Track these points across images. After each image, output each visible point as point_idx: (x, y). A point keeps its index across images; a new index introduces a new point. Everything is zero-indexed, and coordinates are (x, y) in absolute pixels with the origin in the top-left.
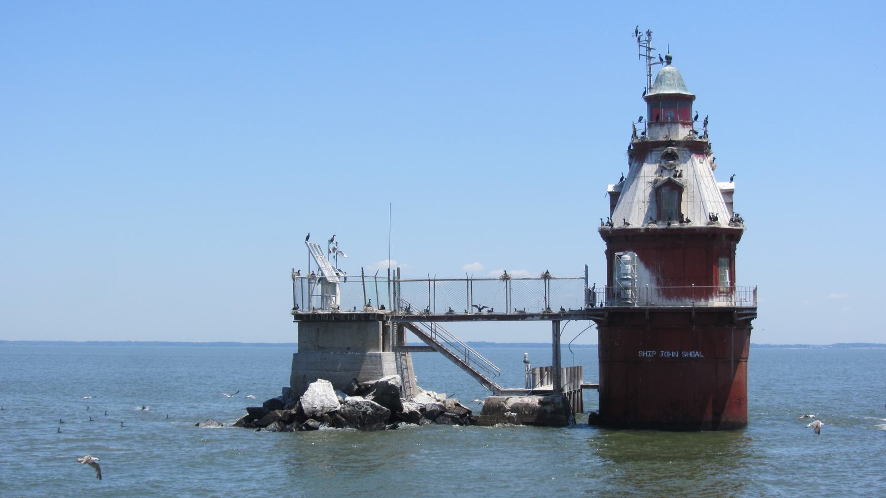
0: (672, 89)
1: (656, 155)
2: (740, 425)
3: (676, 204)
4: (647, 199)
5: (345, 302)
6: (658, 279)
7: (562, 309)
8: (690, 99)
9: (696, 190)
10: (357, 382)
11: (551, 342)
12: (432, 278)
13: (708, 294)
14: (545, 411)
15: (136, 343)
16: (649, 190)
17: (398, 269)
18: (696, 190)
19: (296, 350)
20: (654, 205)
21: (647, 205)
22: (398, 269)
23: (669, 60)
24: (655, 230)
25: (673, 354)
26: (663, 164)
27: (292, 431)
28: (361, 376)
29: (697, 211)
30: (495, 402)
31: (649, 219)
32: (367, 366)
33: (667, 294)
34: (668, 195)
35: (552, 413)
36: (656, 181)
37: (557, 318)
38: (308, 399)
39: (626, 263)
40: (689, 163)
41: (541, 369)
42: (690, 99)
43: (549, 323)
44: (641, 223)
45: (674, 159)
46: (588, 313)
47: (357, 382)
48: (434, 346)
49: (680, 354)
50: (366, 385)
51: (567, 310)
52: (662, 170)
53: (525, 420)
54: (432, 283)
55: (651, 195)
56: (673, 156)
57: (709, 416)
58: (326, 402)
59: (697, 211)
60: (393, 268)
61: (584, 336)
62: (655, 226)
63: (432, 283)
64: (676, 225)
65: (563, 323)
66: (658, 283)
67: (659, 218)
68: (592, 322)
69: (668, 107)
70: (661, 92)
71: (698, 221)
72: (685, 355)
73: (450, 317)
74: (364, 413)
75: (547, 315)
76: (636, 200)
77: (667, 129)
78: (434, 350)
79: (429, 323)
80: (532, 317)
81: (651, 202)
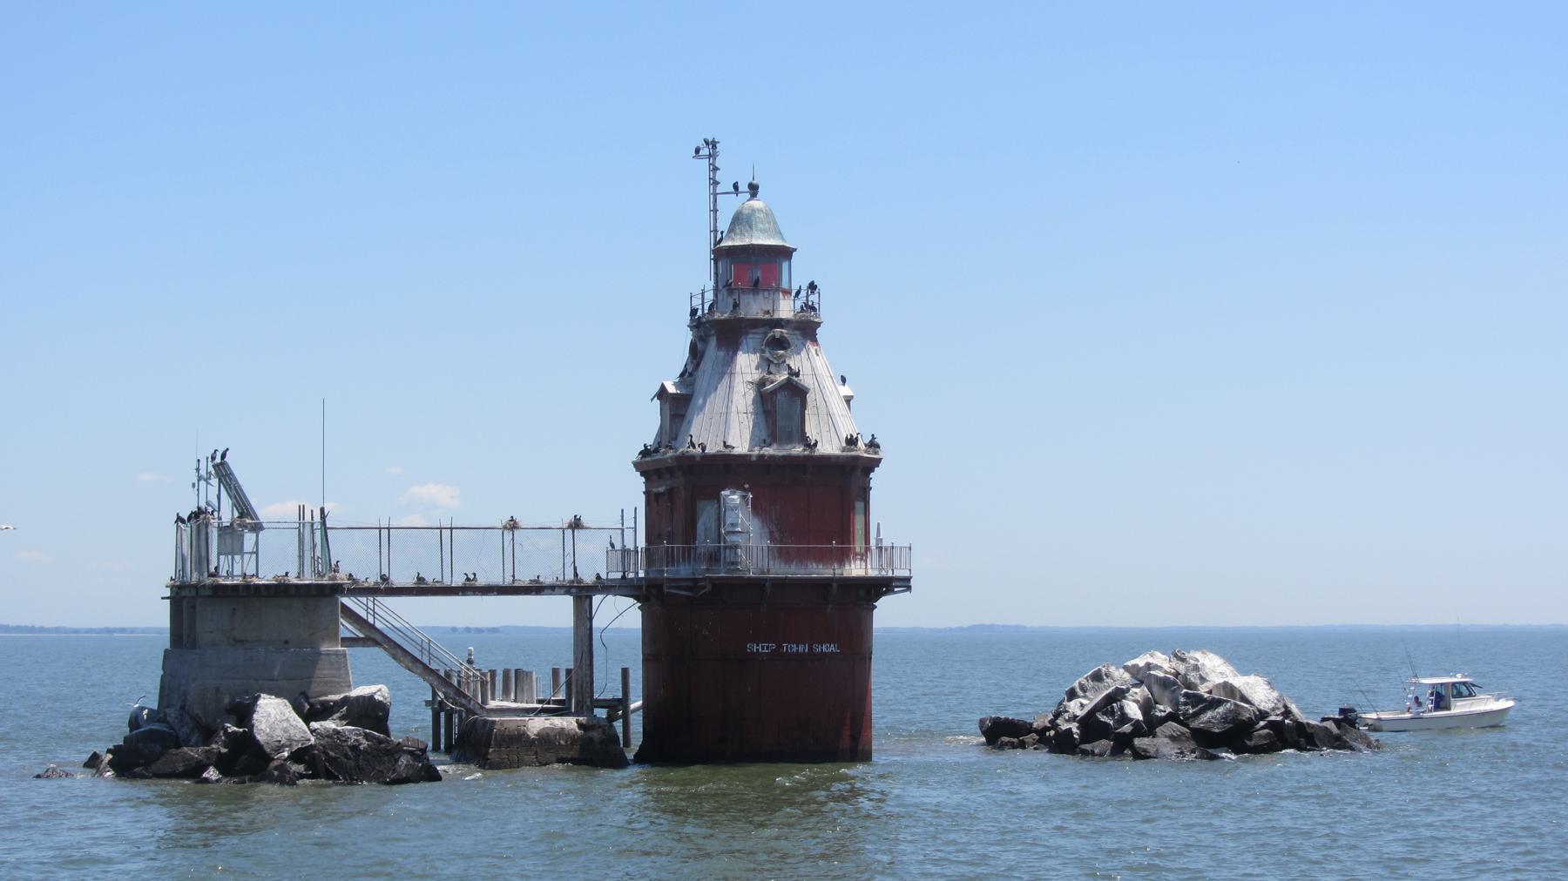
0: (770, 237)
1: (752, 339)
2: (859, 752)
3: (797, 418)
4: (750, 409)
5: (273, 560)
6: (771, 533)
7: (598, 577)
8: (786, 253)
9: (819, 397)
10: (307, 698)
11: (640, 625)
12: (384, 524)
13: (844, 556)
14: (591, 740)
15: (58, 630)
16: (751, 395)
17: (322, 510)
18: (819, 397)
19: (166, 642)
20: (762, 418)
21: (751, 418)
22: (322, 510)
23: (754, 189)
24: (772, 457)
25: (801, 649)
26: (767, 355)
27: (434, 776)
28: (315, 688)
29: (824, 429)
30: (512, 727)
31: (755, 440)
32: (323, 671)
33: (785, 556)
34: (782, 404)
35: (602, 742)
36: (761, 384)
37: (582, 593)
38: (263, 726)
39: (735, 508)
40: (804, 353)
41: (506, 673)
42: (786, 253)
43: (568, 600)
44: (747, 445)
45: (784, 348)
46: (623, 587)
47: (307, 698)
48: (378, 637)
49: (811, 648)
50: (324, 703)
51: (429, 580)
52: (767, 364)
53: (562, 754)
54: (385, 532)
55: (754, 401)
56: (782, 344)
57: (846, 743)
58: (292, 732)
59: (824, 429)
60: (313, 508)
61: (620, 617)
62: (769, 451)
63: (446, 533)
64: (798, 450)
65: (597, 599)
66: (772, 539)
67: (773, 437)
68: (632, 601)
69: (748, 266)
70: (755, 242)
71: (829, 446)
72: (818, 649)
73: (421, 589)
74: (354, 748)
75: (566, 589)
76: (734, 409)
77: (747, 303)
78: (377, 643)
79: (364, 599)
80: (552, 589)
81: (756, 414)
